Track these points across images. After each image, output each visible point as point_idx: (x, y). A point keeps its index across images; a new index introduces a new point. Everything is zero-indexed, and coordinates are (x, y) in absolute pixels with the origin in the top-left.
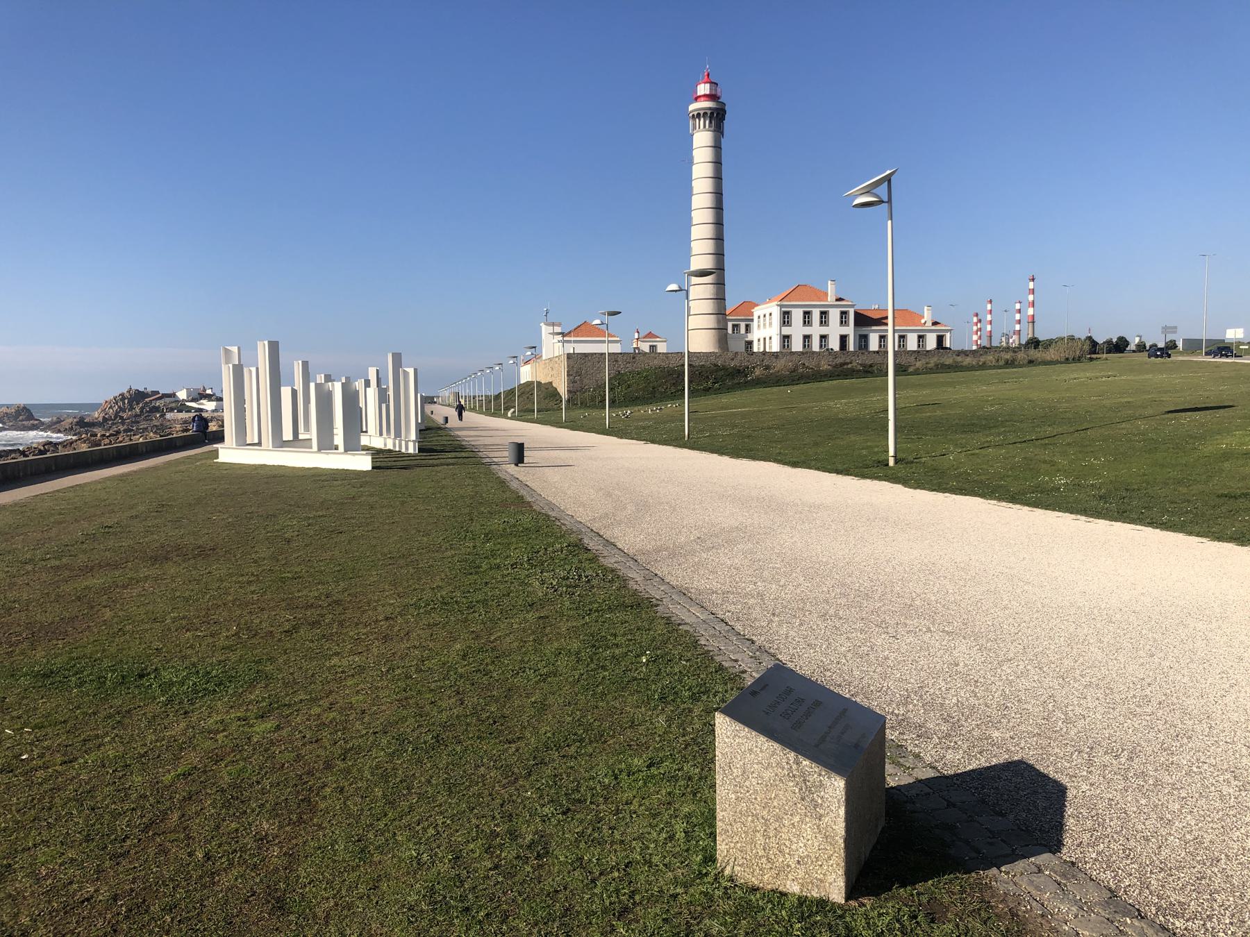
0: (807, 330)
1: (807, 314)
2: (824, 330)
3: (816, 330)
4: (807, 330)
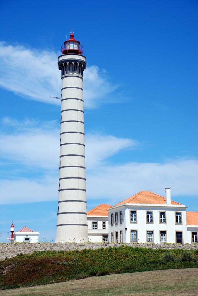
0: (150, 227)
2: (134, 227)
3: (157, 227)
4: (150, 227)
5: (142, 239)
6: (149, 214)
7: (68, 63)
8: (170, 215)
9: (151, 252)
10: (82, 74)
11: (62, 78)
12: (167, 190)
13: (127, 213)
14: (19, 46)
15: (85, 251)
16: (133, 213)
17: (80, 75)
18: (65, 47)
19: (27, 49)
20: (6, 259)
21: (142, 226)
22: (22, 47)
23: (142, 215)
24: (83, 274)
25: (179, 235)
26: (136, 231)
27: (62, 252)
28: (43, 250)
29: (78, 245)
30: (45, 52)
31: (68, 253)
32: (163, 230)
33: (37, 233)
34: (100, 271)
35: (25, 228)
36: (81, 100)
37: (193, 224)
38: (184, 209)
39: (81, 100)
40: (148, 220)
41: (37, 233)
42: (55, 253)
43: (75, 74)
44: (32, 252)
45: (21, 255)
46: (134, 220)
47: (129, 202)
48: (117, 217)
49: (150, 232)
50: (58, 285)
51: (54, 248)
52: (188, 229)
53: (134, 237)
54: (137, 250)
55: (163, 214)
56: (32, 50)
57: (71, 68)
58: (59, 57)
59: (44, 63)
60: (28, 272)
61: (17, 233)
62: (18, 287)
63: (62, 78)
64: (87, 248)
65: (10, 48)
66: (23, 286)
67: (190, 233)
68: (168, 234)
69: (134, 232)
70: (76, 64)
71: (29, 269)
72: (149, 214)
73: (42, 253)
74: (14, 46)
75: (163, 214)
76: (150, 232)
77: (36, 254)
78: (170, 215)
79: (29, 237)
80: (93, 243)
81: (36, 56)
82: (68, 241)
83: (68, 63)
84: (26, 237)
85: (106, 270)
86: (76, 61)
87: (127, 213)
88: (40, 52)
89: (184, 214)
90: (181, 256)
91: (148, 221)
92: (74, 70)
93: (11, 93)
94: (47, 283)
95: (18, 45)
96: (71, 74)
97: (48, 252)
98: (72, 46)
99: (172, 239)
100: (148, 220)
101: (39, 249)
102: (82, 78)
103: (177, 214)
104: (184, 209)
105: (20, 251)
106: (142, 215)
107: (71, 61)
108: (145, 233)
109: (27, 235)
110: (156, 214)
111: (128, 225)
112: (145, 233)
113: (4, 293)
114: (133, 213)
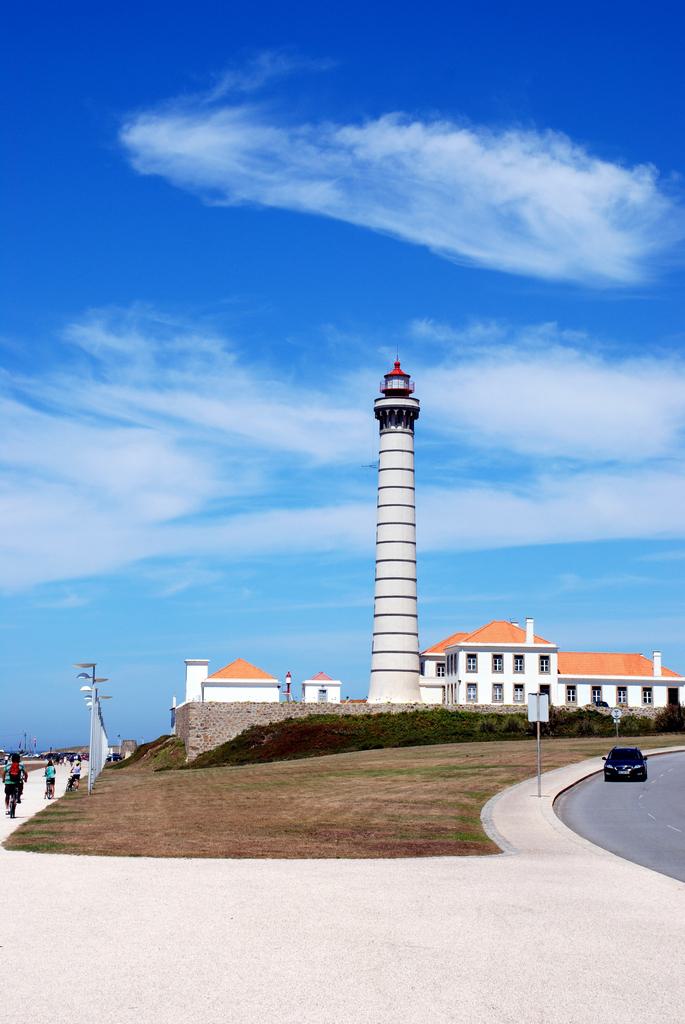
0: (498, 678)
2: (472, 678)
3: (509, 678)
4: (498, 678)
5: (485, 698)
6: (497, 658)
7: (388, 411)
8: (532, 661)
9: (475, 717)
10: (412, 428)
11: (381, 434)
12: (528, 621)
13: (462, 657)
14: (440, 122)
15: (380, 715)
16: (472, 657)
17: (408, 430)
18: (386, 384)
19: (461, 129)
20: (271, 723)
21: (485, 676)
22: (448, 124)
23: (485, 660)
24: (353, 748)
26: (475, 685)
27: (348, 716)
28: (322, 713)
29: (370, 707)
30: (512, 136)
31: (355, 718)
32: (518, 682)
33: (339, 682)
34: (374, 743)
35: (321, 675)
36: (409, 470)
37: (570, 673)
38: (554, 650)
39: (409, 470)
41: (339, 682)
42: (338, 717)
43: (400, 428)
44: (306, 715)
45: (291, 718)
46: (472, 668)
47: (466, 641)
48: (447, 665)
49: (499, 686)
50: (447, 773)
51: (337, 711)
52: (560, 681)
53: (472, 693)
54: (456, 714)
55: (519, 658)
56: (473, 132)
57: (394, 422)
58: (376, 400)
59: (507, 165)
60: (292, 742)
62: (271, 761)
63: (381, 434)
64: (384, 711)
65: (416, 129)
66: (276, 760)
67: (563, 687)
69: (472, 686)
70: (400, 412)
71: (293, 739)
72: (497, 658)
73: (318, 716)
74: (427, 122)
75: (519, 658)
76: (499, 686)
77: (311, 718)
78: (532, 661)
79: (325, 688)
80: (393, 705)
81: (487, 147)
82: (384, 701)
83: (388, 411)
84: (321, 688)
85: (380, 742)
86: (401, 408)
87: (462, 657)
88: (496, 135)
89: (554, 658)
90: (505, 724)
92: (397, 423)
93: (423, 251)
95: (438, 119)
96: (393, 428)
97: (328, 715)
98: (397, 384)
101: (315, 712)
102: (412, 435)
103: (542, 658)
104: (554, 650)
105: (289, 713)
106: (485, 660)
107: (392, 408)
108: (491, 686)
109: (323, 686)
110: (508, 658)
111: (463, 675)
112: (512, 687)
114: (472, 657)
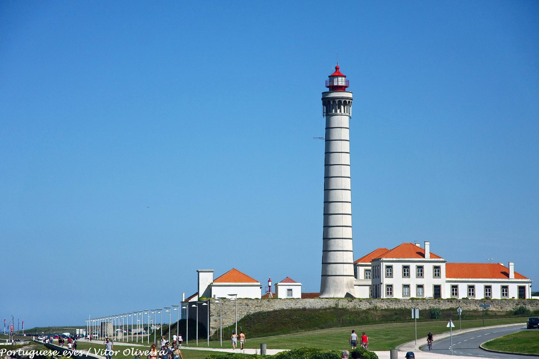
0: (406, 281)
1: (406, 269)
2: (420, 281)
3: (413, 281)
4: (406, 281)
25: (437, 289)
32: (420, 283)
33: (300, 284)
35: (288, 280)
40: (405, 274)
41: (370, 264)
49: (407, 286)
61: (279, 284)
68: (425, 287)
78: (428, 269)
91: (436, 275)
94: (328, 311)
99: (429, 293)
100: (405, 274)
108: (401, 287)
113: (298, 340)
